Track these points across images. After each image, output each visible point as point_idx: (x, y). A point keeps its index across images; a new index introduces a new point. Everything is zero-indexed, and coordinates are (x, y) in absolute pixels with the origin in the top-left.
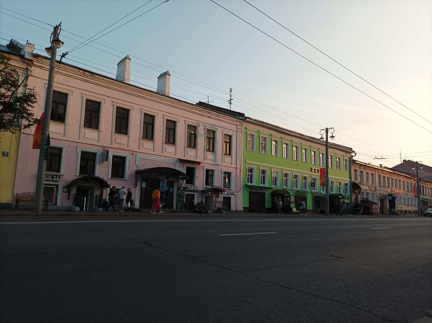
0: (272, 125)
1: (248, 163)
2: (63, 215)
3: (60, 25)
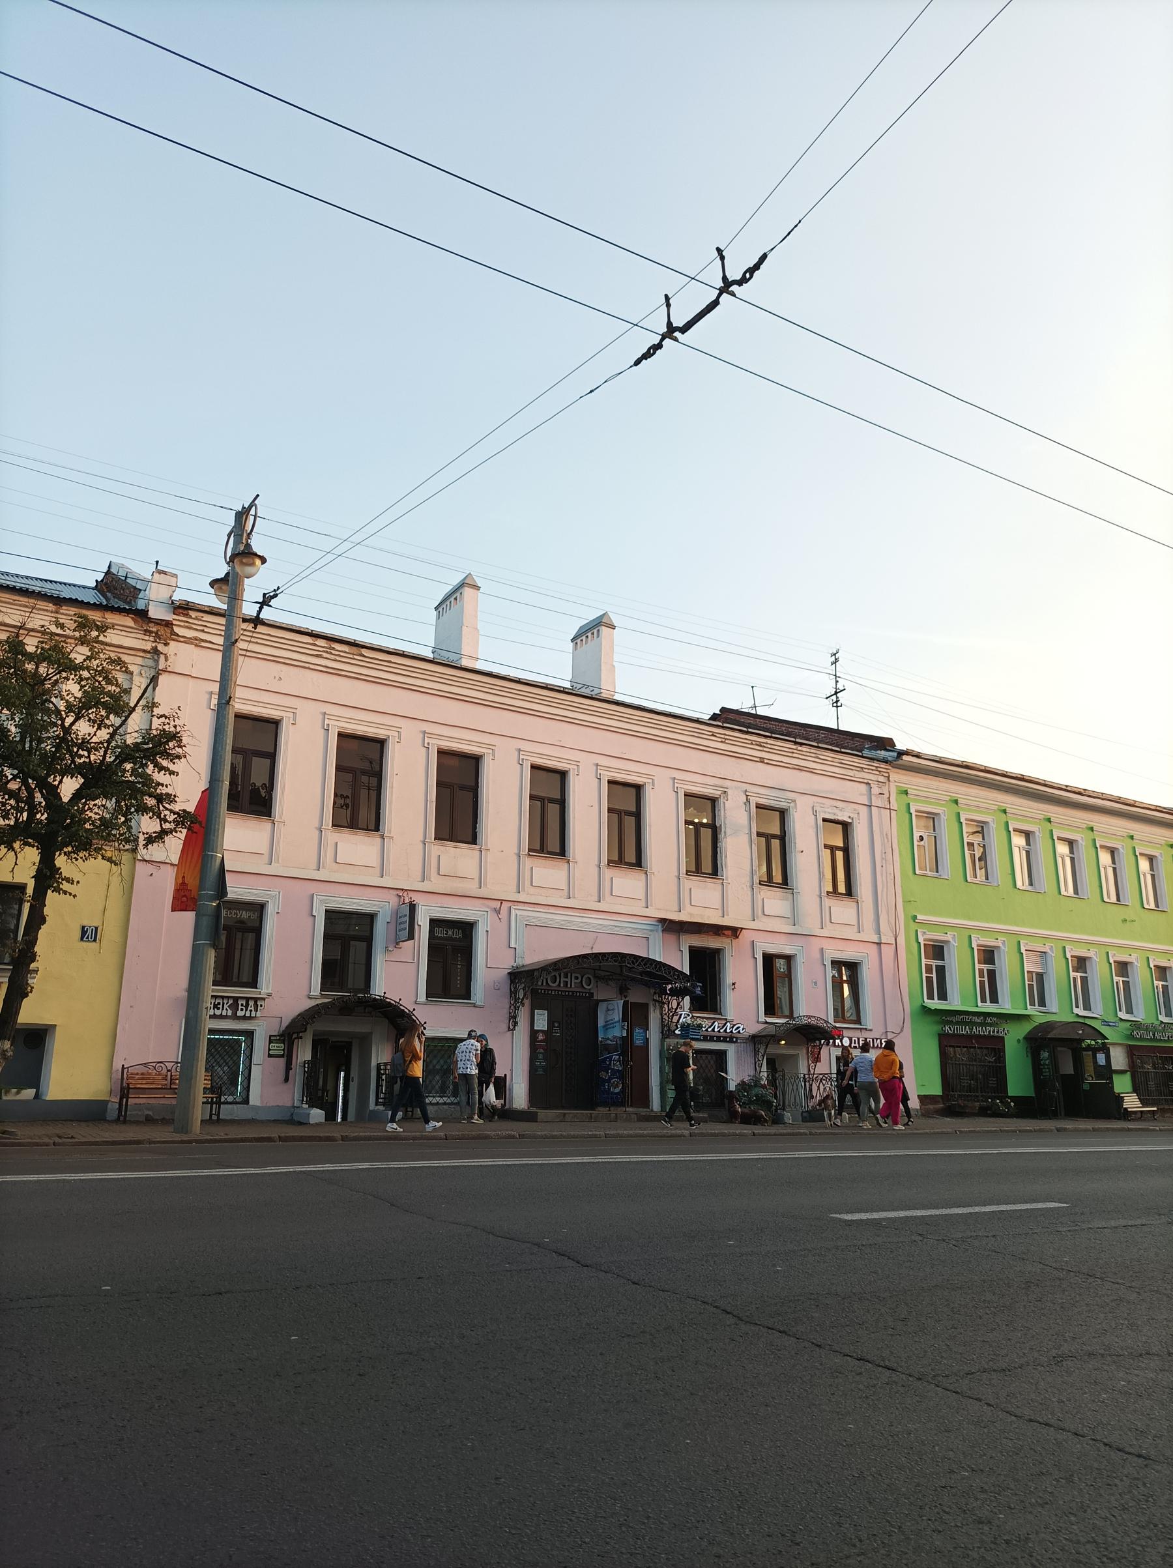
0: (986, 771)
2: (269, 1139)
3: (253, 504)
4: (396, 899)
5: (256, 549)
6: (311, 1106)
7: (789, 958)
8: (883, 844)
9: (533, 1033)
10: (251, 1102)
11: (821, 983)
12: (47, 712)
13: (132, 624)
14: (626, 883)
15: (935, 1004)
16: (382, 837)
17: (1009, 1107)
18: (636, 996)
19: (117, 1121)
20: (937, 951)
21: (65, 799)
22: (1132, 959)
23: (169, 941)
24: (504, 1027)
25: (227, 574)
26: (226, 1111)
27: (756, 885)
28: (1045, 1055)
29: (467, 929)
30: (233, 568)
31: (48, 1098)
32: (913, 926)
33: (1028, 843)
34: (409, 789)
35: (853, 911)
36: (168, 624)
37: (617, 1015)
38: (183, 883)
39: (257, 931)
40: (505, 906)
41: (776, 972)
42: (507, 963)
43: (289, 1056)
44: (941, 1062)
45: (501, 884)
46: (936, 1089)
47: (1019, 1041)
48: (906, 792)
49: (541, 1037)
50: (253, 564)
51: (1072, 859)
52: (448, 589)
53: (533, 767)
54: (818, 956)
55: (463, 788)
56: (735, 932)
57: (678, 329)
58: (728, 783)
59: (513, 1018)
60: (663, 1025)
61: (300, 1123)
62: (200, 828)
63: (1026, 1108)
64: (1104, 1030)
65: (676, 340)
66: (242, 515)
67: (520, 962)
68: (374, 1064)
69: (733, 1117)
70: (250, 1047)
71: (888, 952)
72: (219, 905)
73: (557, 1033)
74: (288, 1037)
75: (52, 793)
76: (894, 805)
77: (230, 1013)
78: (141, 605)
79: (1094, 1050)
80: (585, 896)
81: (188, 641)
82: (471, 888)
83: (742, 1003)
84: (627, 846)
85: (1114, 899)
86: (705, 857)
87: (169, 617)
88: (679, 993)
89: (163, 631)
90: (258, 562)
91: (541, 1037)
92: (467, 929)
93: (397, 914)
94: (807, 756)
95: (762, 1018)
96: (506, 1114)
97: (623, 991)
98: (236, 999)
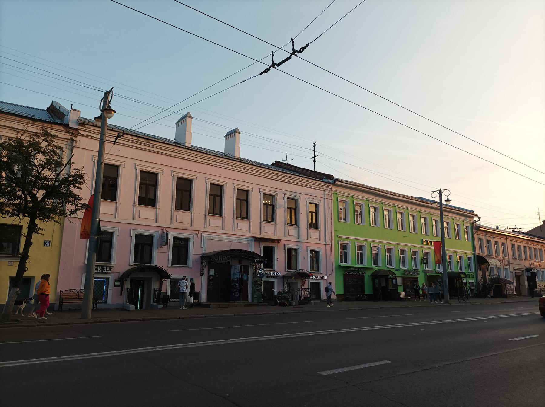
1: (341, 238)
3: (111, 90)
4: (161, 230)
5: (112, 107)
6: (130, 304)
7: (296, 250)
8: (328, 211)
9: (209, 277)
10: (108, 302)
11: (306, 258)
12: (31, 165)
13: (63, 129)
14: (242, 225)
15: (343, 264)
16: (156, 209)
17: (365, 298)
18: (245, 263)
19: (58, 311)
20: (344, 247)
21: (39, 199)
22: (406, 249)
23: (78, 250)
24: (199, 274)
25: (101, 115)
26: (99, 306)
27: (286, 225)
28: (377, 281)
29: (186, 241)
30: (103, 114)
32: (337, 239)
33: (375, 211)
34: (166, 191)
35: (318, 234)
36: (77, 130)
37: (238, 270)
38: (85, 229)
39: (110, 242)
40: (200, 233)
41: (292, 254)
42: (200, 253)
43: (122, 286)
45: (198, 225)
46: (342, 292)
48: (337, 194)
49: (211, 278)
50: (111, 113)
51: (389, 216)
52: (181, 117)
53: (211, 184)
54: (306, 249)
55: (186, 191)
56: (279, 241)
57: (276, 64)
58: (278, 190)
59: (202, 273)
60: (253, 273)
61: (126, 310)
62: (91, 209)
63: (371, 298)
64: (396, 272)
66: (107, 94)
67: (205, 252)
68: (152, 288)
69: (276, 304)
70: (108, 283)
71: (328, 247)
72: (98, 238)
73: (217, 276)
74: (121, 279)
75: (34, 197)
76: (333, 198)
77: (100, 271)
78: (66, 122)
79: (392, 279)
80: (228, 229)
81: (84, 136)
82: (188, 226)
83: (280, 265)
84: (243, 212)
85: (401, 229)
86: (269, 215)
87: (77, 127)
88: (259, 262)
89: (75, 132)
90: (113, 113)
91: (211, 278)
92: (186, 241)
93: (161, 236)
94: (305, 181)
95: (287, 270)
96: (199, 305)
97: (240, 262)
98: (103, 267)
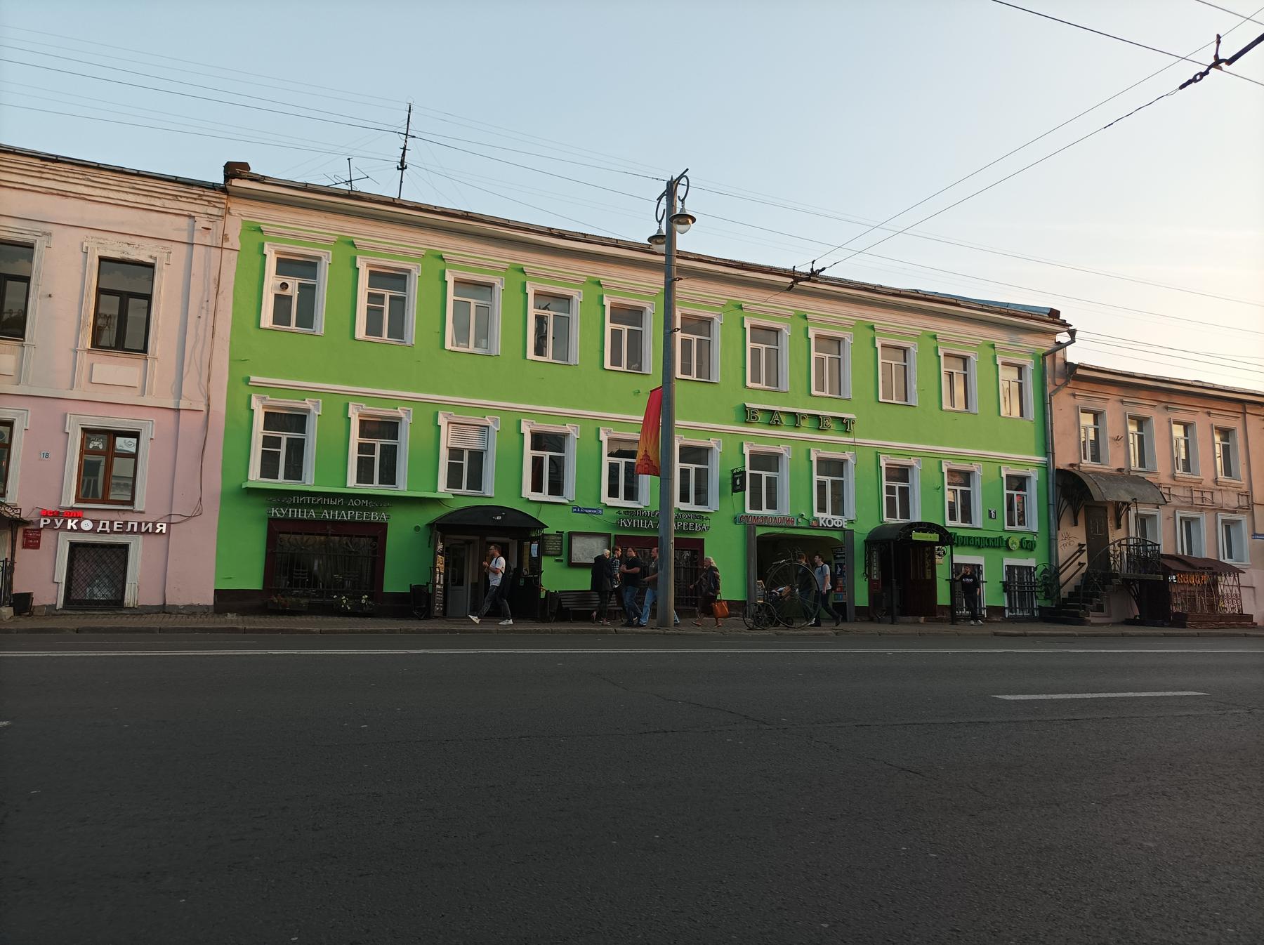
0: (445, 213)
1: (260, 388)
2: (394, 632)
3: (682, 176)
31: (212, 603)
44: (268, 546)
47: (417, 529)
65: (1221, 69)
